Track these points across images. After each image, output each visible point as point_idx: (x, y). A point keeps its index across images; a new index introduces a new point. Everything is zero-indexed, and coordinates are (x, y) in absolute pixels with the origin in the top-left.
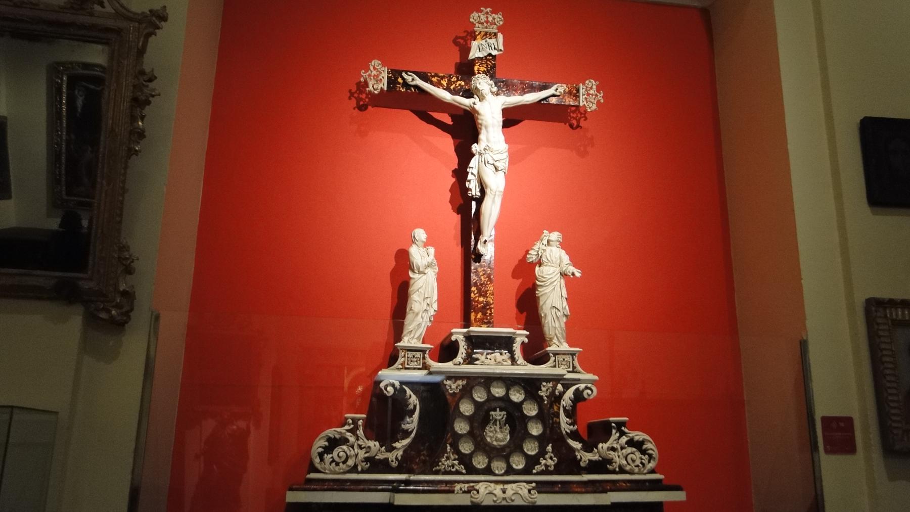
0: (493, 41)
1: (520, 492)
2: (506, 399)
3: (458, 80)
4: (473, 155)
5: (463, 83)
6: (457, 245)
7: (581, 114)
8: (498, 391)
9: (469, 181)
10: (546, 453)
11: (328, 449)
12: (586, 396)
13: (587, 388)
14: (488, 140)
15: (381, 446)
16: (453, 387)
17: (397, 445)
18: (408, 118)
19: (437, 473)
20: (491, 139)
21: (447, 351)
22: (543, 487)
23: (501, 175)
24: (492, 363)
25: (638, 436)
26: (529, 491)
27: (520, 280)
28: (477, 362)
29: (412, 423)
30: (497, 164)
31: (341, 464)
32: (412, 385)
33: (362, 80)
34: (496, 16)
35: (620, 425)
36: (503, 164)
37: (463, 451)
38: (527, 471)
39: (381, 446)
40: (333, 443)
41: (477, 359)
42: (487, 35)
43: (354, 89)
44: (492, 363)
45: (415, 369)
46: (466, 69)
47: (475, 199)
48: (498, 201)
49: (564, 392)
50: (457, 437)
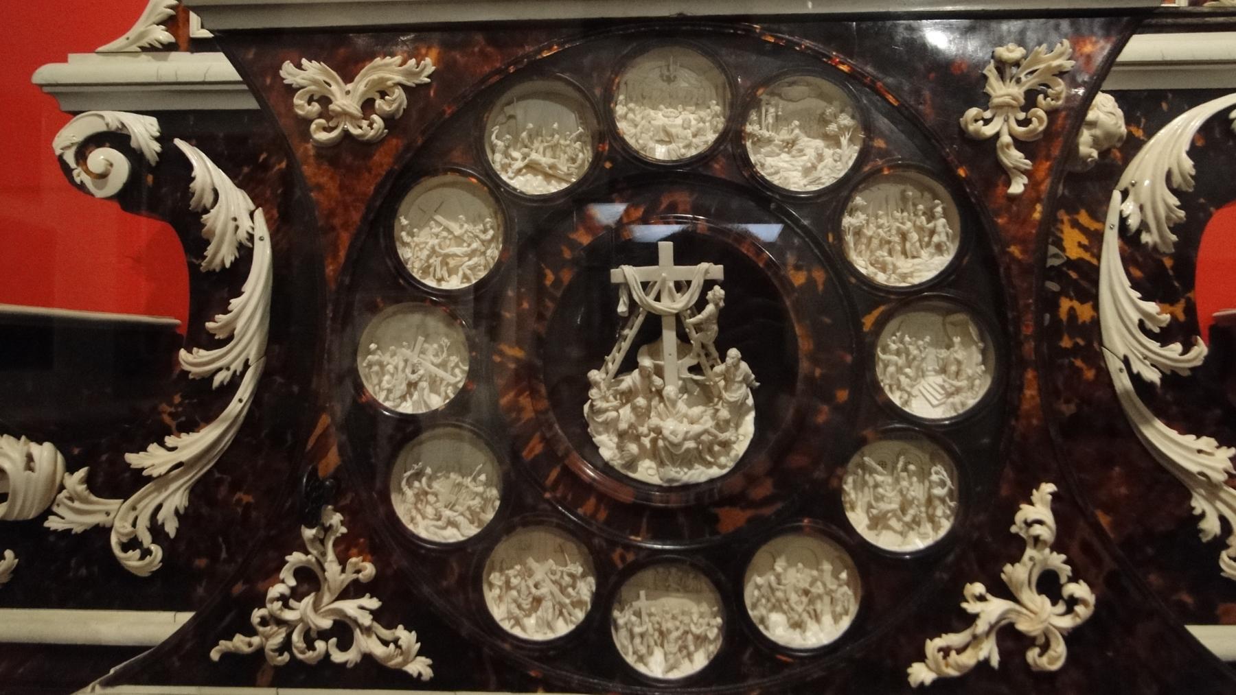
2: (723, 179)
10: (1014, 548)
17: (153, 459)
49: (1131, 146)
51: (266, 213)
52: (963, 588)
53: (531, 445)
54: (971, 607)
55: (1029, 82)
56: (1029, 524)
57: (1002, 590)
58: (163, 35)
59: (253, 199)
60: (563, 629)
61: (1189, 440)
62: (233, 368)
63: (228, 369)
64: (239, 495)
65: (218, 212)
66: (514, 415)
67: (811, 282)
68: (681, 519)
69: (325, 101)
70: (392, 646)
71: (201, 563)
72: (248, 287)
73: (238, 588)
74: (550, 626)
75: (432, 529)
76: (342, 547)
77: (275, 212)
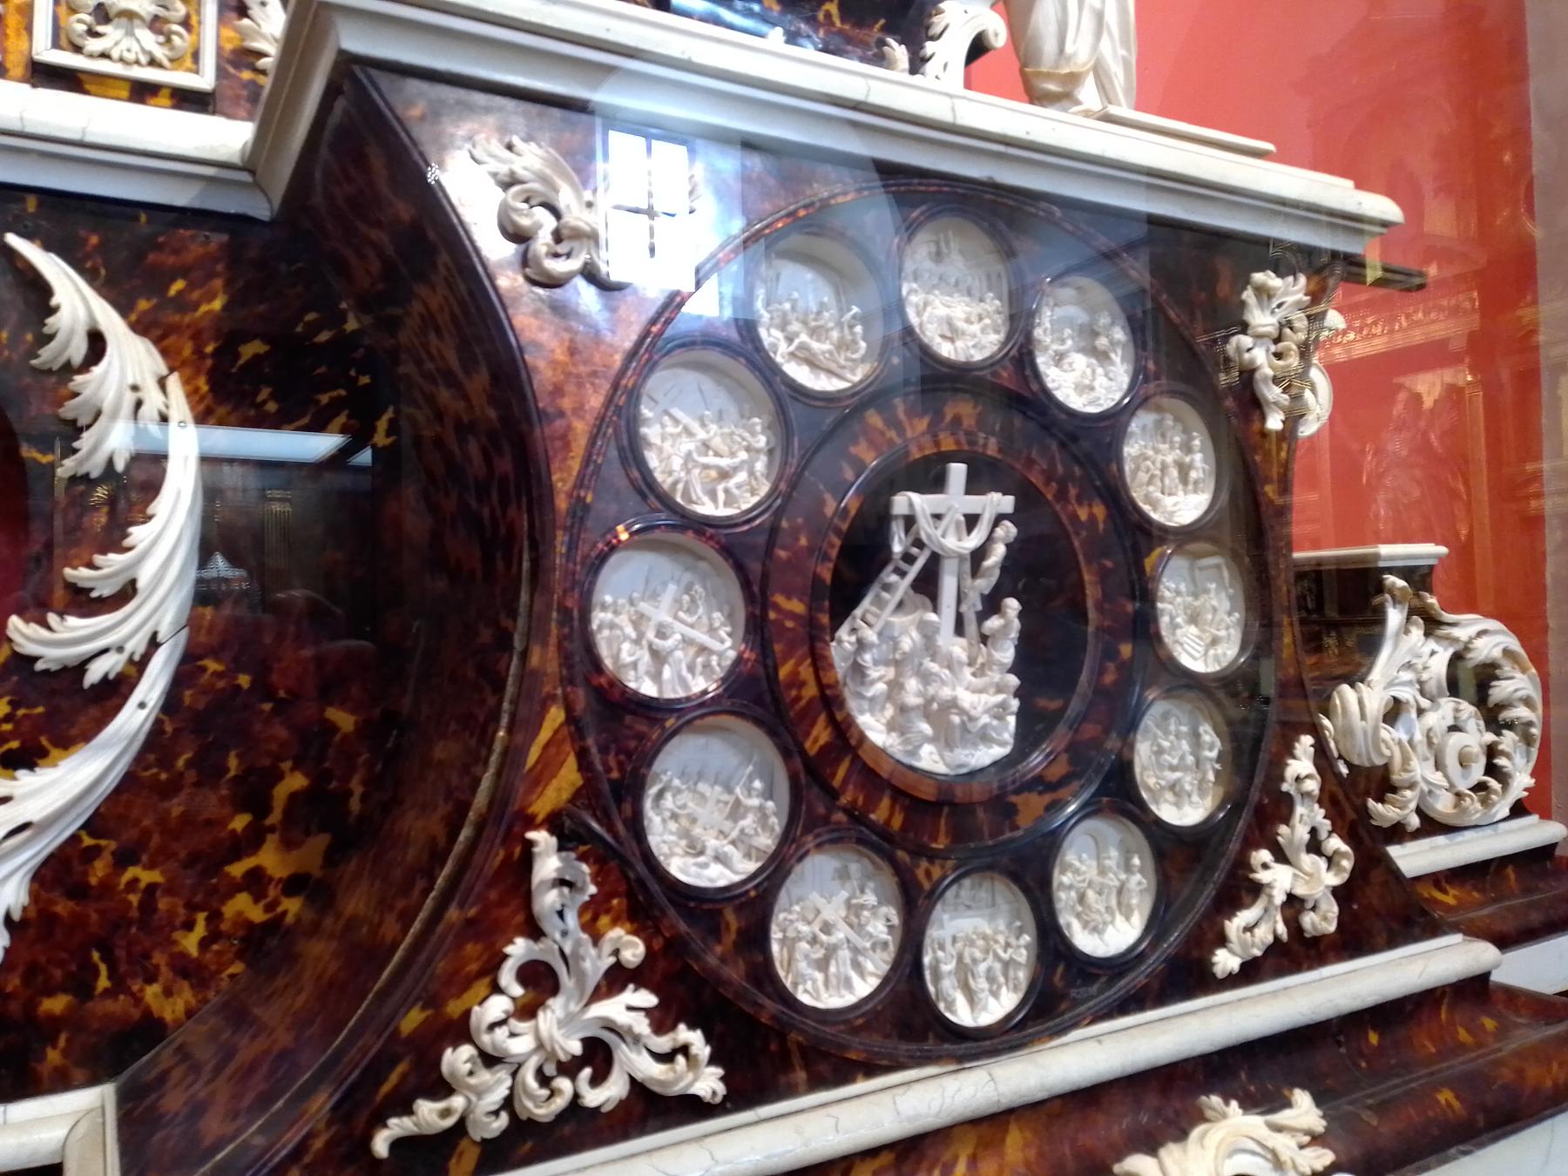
2: (1012, 386)
35: (1418, 577)
37: (681, 868)
38: (1178, 972)
50: (627, 731)
51: (186, 382)
52: (1249, 858)
53: (815, 732)
54: (1262, 876)
56: (1298, 779)
57: (1281, 857)
59: (165, 353)
60: (864, 987)
62: (129, 647)
63: (120, 649)
64: (132, 872)
65: (107, 372)
66: (794, 693)
67: (1092, 517)
68: (981, 814)
70: (680, 1059)
71: (56, 1004)
72: (161, 506)
73: (413, 1019)
74: (848, 984)
75: (694, 869)
76: (587, 916)
77: (203, 384)
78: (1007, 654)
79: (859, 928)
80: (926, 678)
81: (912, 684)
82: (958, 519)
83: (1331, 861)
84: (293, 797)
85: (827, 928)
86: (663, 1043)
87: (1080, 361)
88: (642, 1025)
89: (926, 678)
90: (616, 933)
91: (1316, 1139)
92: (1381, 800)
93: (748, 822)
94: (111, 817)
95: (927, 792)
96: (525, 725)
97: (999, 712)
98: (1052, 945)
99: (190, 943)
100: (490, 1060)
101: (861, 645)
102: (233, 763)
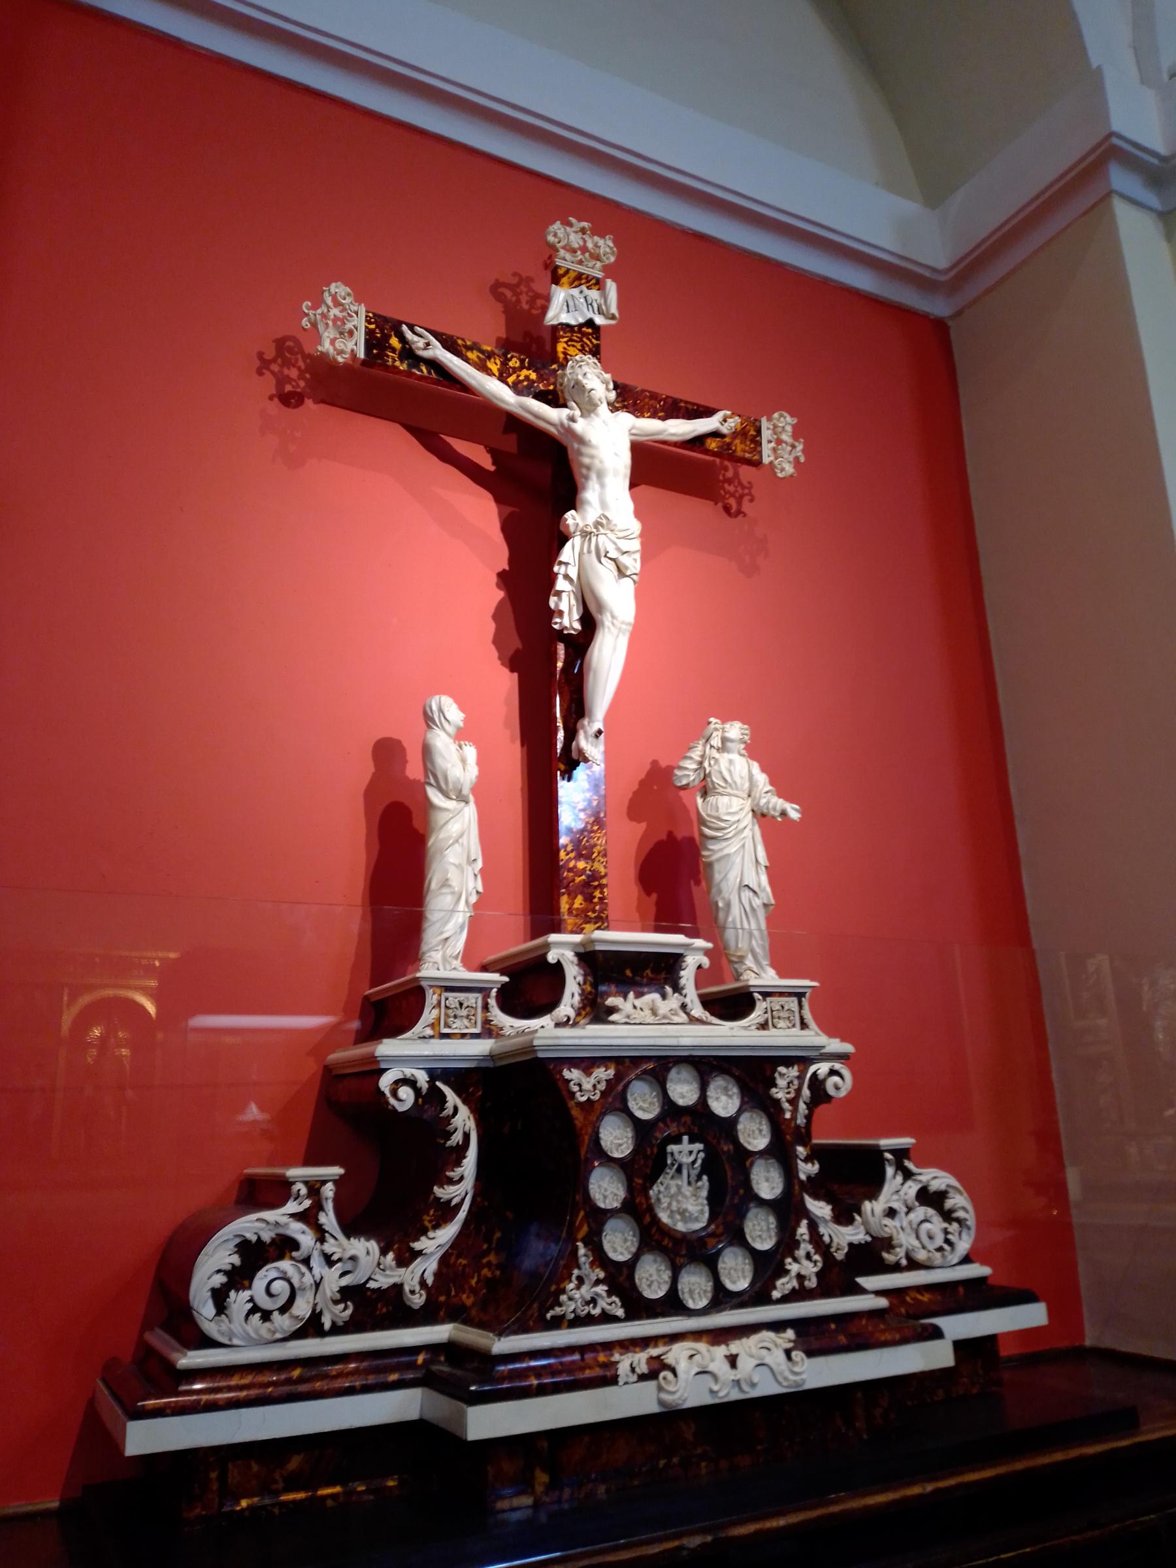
0: (594, 294)
1: (768, 1360)
2: (701, 1109)
3: (522, 367)
4: (563, 539)
5: (533, 376)
6: (513, 741)
7: (743, 487)
8: (683, 1091)
9: (559, 594)
11: (239, 1277)
12: (831, 1091)
13: (833, 1072)
14: (603, 504)
15: (384, 1252)
16: (586, 1085)
18: (392, 440)
19: (557, 1323)
20: (609, 499)
21: (529, 987)
22: (815, 1337)
23: (628, 585)
24: (646, 1022)
25: (937, 1179)
26: (788, 1353)
27: (643, 825)
28: (614, 1017)
29: (461, 1186)
30: (625, 560)
31: (276, 1316)
32: (463, 1078)
33: (305, 322)
34: (601, 242)
35: (900, 1154)
36: (633, 564)
38: (759, 1295)
39: (384, 1252)
40: (254, 1256)
41: (613, 1010)
42: (579, 280)
43: (270, 354)
44: (646, 1022)
45: (463, 1036)
46: (536, 351)
47: (567, 639)
48: (623, 643)
50: (599, 1217)
54: (788, 1267)
55: (788, 1080)
57: (796, 1260)
58: (429, 1032)
60: (661, 1294)
61: (816, 1203)
64: (460, 1260)
69: (580, 1085)
71: (442, 1298)
73: (553, 1288)
78: (704, 1193)
79: (660, 1276)
80: (678, 1202)
81: (674, 1204)
82: (687, 1152)
83: (815, 1262)
84: (498, 1239)
85: (651, 1275)
86: (609, 1300)
87: (724, 1098)
88: (604, 1294)
89: (678, 1202)
90: (597, 1270)
91: (790, 1341)
92: (889, 1253)
93: (629, 1243)
94: (458, 1243)
95: (679, 1236)
96: (574, 1216)
97: (702, 1212)
98: (719, 1287)
99: (473, 1282)
100: (570, 1299)
101: (659, 1192)
102: (484, 1228)
